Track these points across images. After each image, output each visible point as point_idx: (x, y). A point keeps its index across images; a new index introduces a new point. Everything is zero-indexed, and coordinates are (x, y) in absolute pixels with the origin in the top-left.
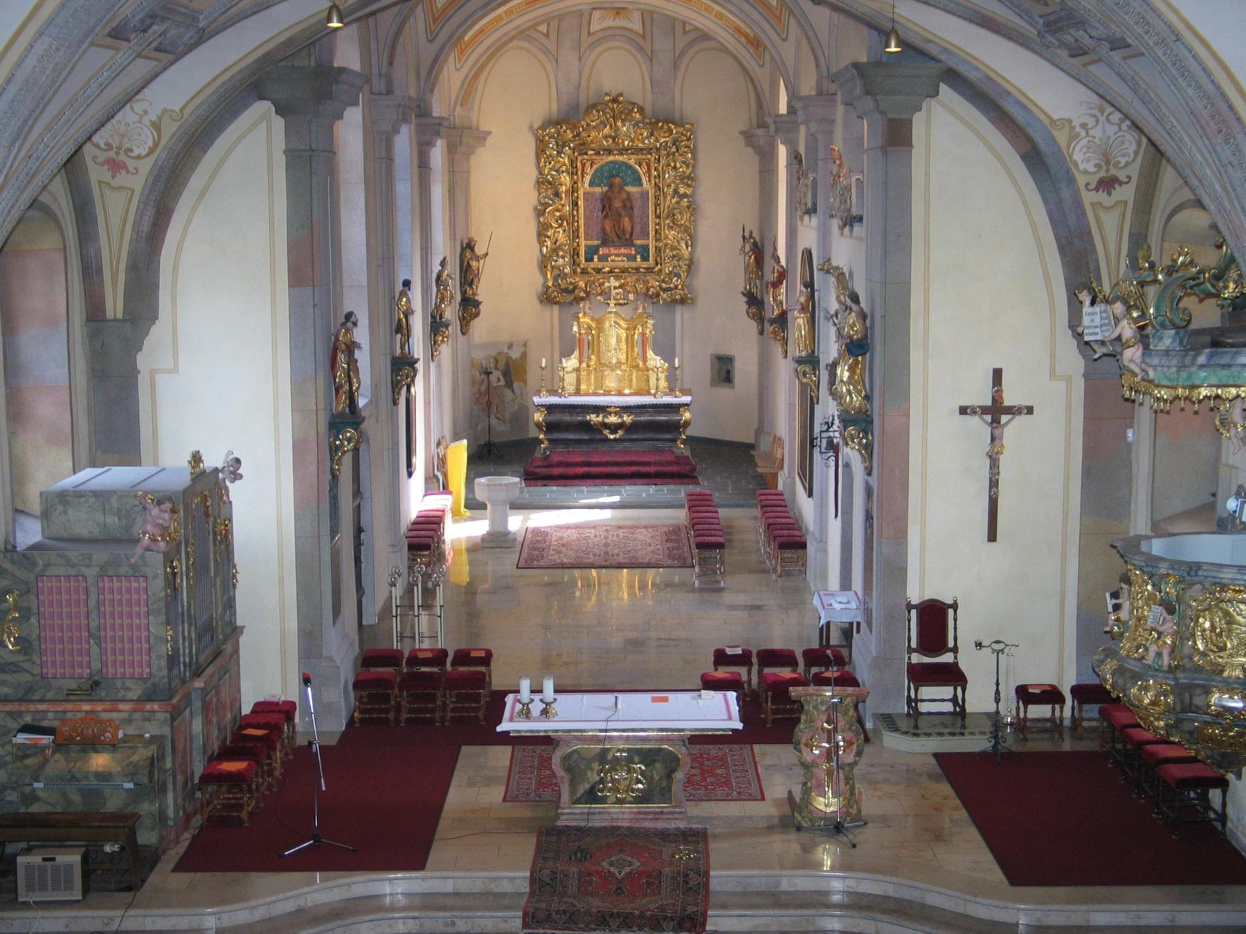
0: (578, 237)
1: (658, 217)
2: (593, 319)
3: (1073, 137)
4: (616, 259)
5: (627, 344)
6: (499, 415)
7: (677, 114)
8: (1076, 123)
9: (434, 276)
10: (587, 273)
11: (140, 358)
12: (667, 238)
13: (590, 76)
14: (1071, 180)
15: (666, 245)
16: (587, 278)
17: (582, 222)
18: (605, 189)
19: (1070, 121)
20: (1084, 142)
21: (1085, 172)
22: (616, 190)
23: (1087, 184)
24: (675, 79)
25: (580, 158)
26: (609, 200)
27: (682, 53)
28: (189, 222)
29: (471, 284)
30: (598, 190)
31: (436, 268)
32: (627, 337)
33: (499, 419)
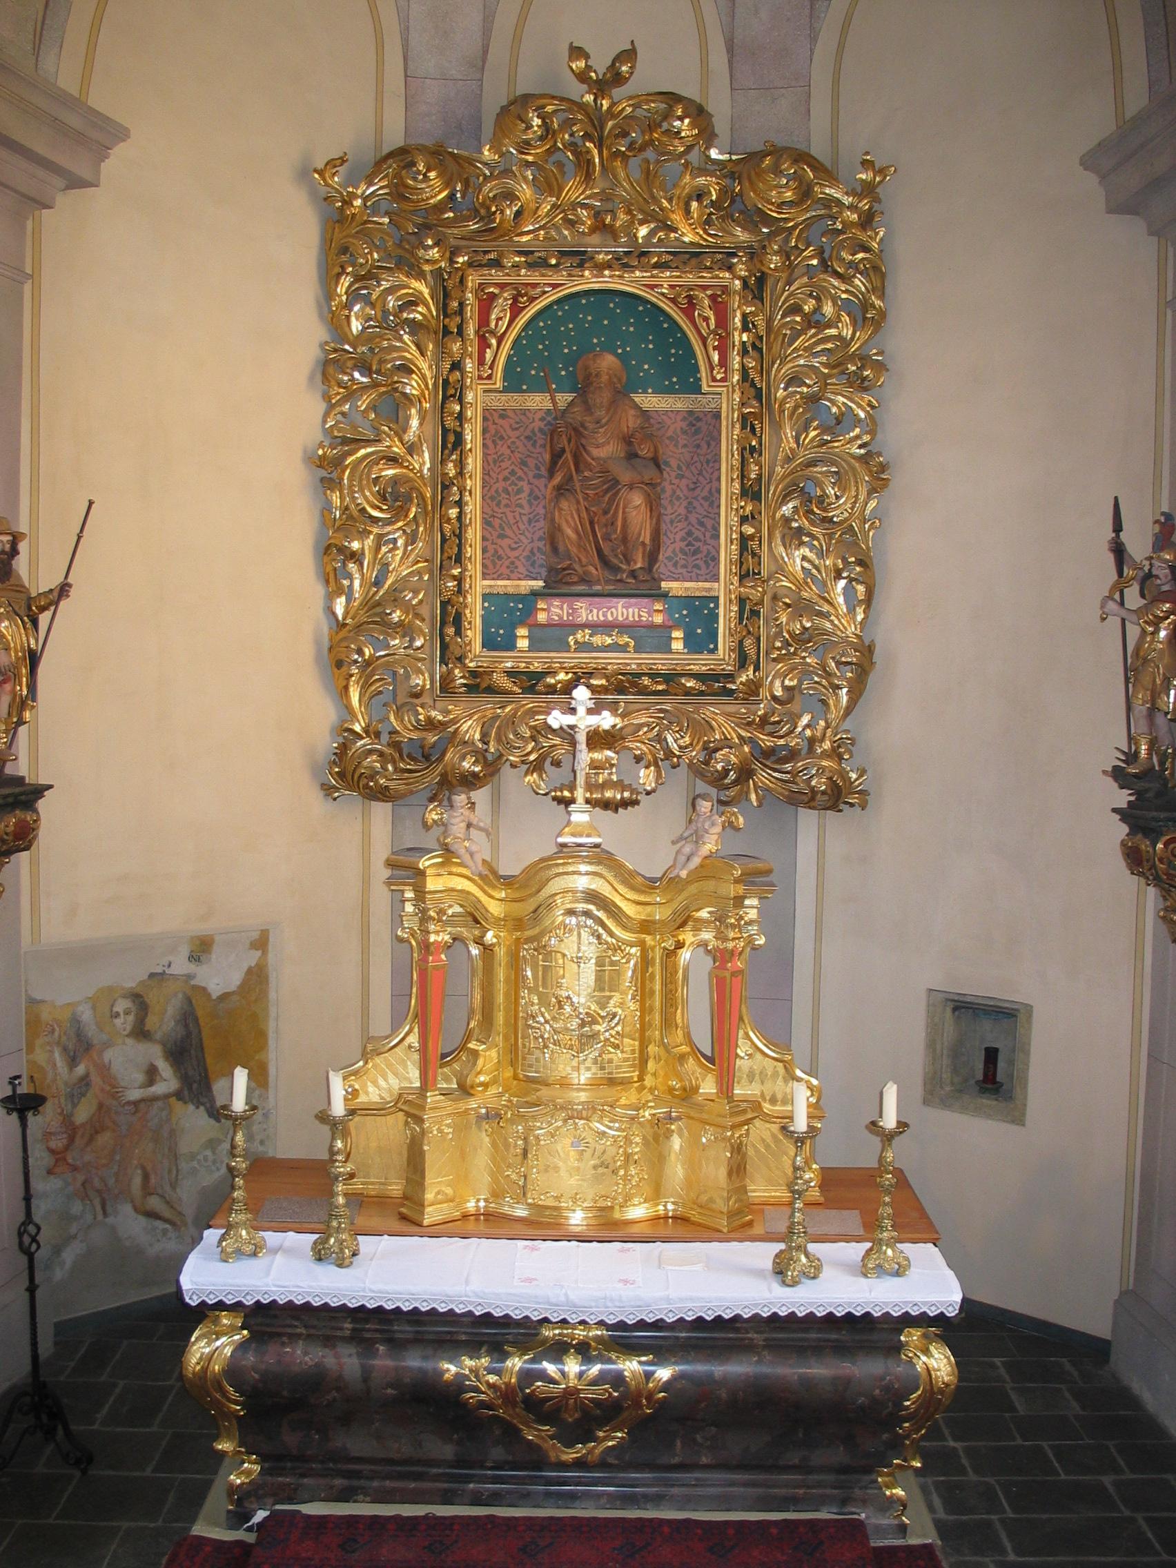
0: (459, 559)
1: (751, 492)
2: (491, 877)
4: (597, 640)
5: (643, 994)
6: (154, 1203)
10: (491, 690)
12: (781, 569)
13: (517, 38)
15: (775, 598)
16: (488, 706)
17: (474, 506)
18: (564, 399)
22: (602, 398)
24: (814, 39)
25: (472, 280)
26: (577, 432)
30: (538, 402)
32: (645, 962)
33: (152, 1215)
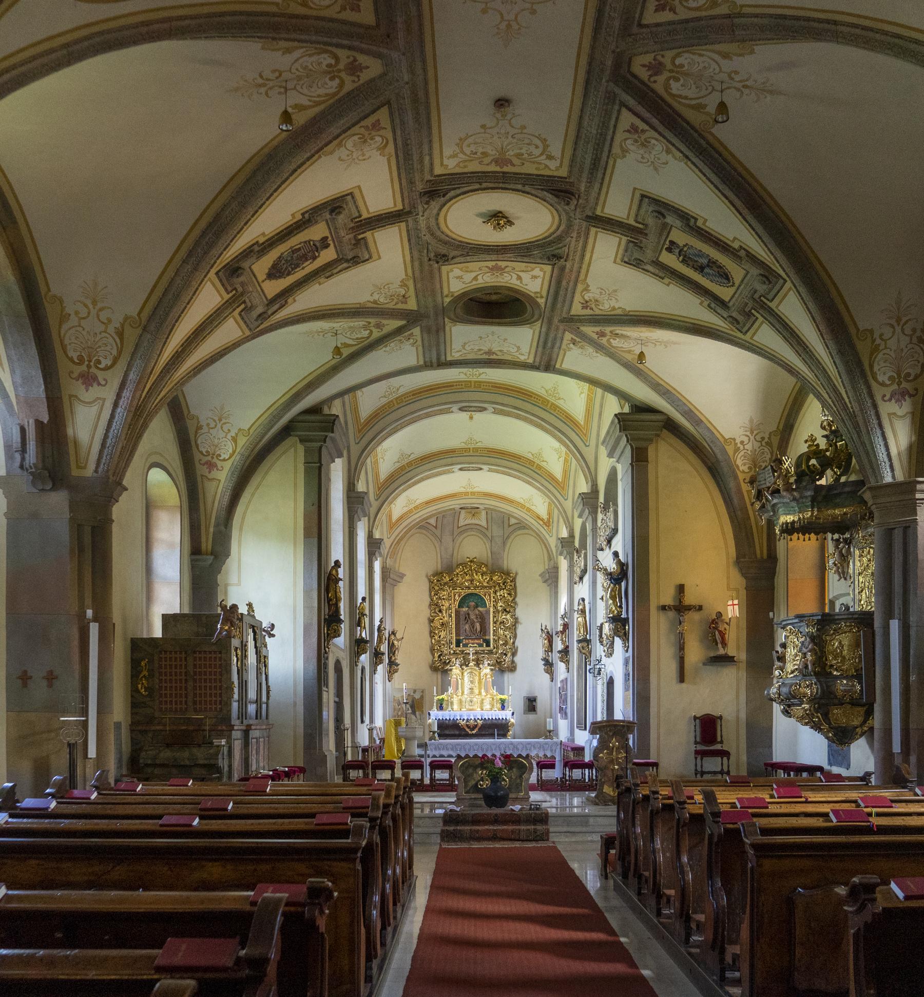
3: (737, 450)
7: (505, 567)
8: (738, 441)
9: (376, 628)
11: (219, 577)
14: (736, 477)
19: (734, 440)
20: (742, 453)
21: (743, 472)
23: (745, 479)
27: (508, 537)
28: (250, 502)
29: (394, 654)
31: (377, 623)
